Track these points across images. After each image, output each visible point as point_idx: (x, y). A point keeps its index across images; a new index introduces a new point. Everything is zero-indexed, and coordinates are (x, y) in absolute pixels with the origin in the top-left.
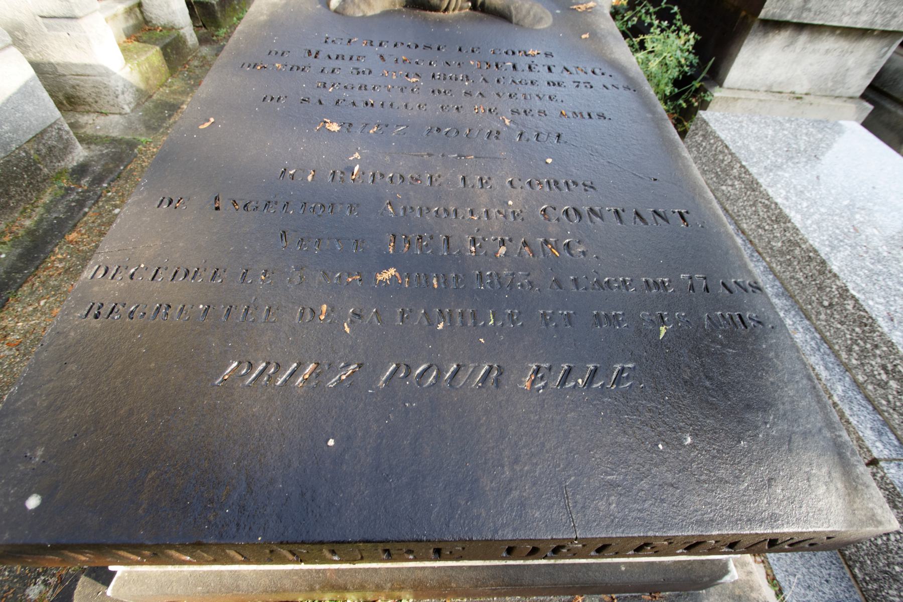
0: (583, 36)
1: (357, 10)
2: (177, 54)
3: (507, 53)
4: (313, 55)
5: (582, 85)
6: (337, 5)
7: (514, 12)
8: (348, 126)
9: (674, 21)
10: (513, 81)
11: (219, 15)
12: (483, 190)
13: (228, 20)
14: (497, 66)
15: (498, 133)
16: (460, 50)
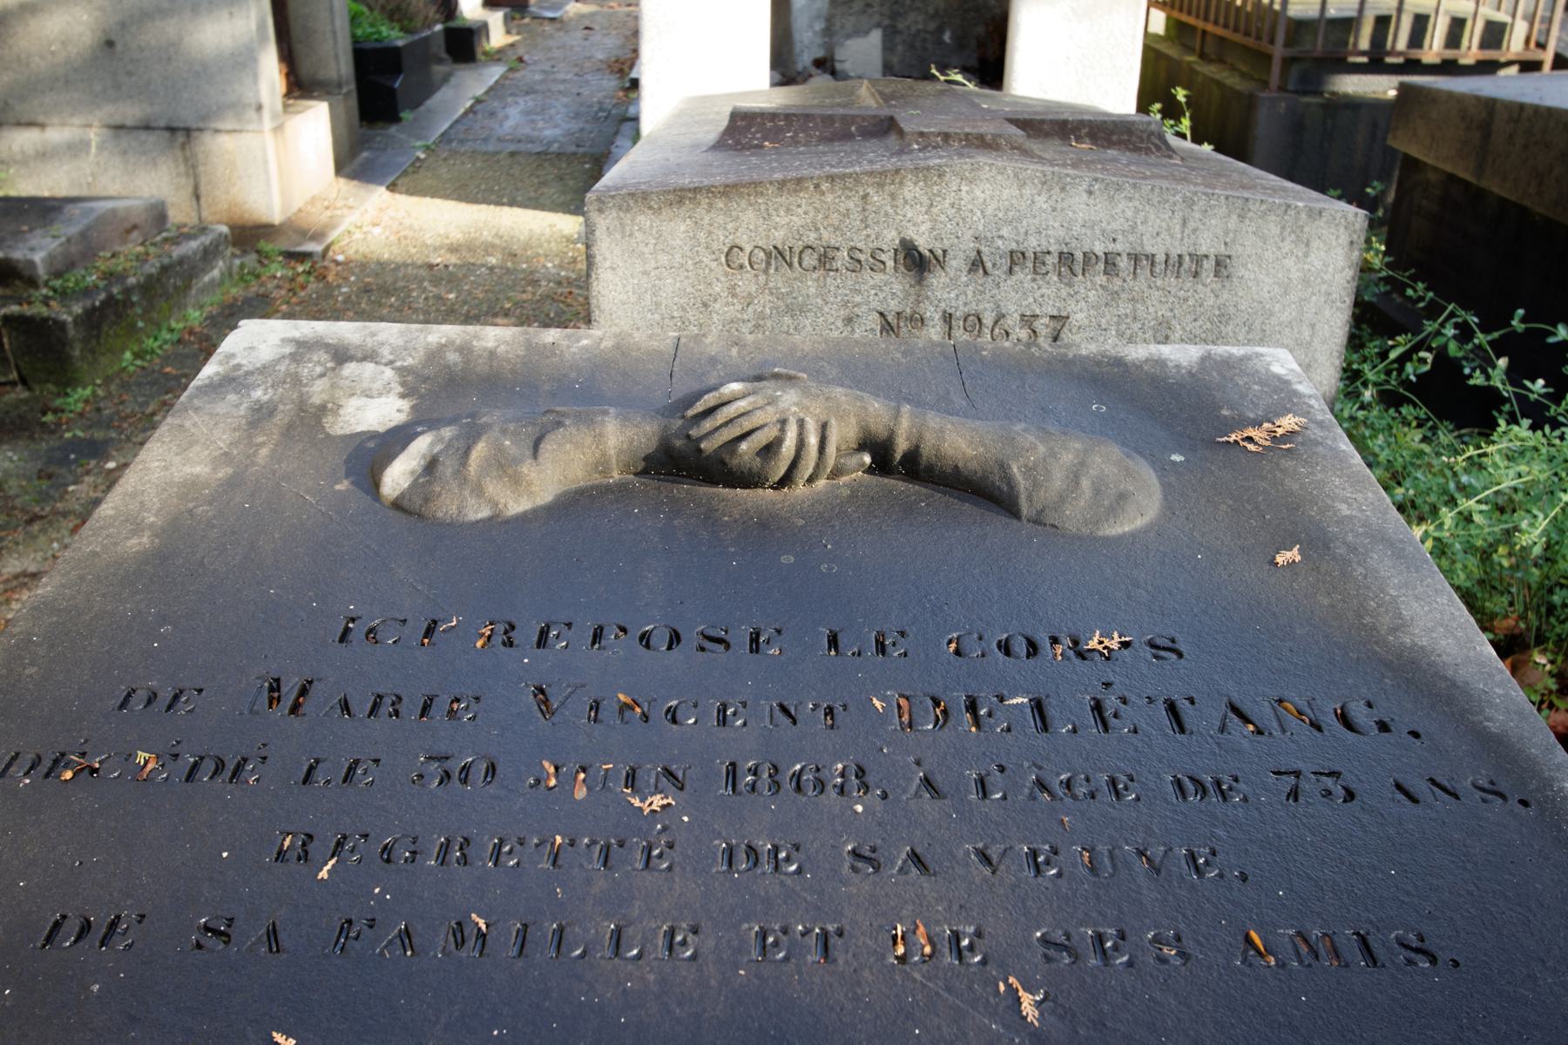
1: (471, 501)
3: (1005, 647)
4: (288, 703)
7: (1022, 483)
10: (1042, 785)
13: (104, 360)
14: (972, 707)
16: (833, 641)
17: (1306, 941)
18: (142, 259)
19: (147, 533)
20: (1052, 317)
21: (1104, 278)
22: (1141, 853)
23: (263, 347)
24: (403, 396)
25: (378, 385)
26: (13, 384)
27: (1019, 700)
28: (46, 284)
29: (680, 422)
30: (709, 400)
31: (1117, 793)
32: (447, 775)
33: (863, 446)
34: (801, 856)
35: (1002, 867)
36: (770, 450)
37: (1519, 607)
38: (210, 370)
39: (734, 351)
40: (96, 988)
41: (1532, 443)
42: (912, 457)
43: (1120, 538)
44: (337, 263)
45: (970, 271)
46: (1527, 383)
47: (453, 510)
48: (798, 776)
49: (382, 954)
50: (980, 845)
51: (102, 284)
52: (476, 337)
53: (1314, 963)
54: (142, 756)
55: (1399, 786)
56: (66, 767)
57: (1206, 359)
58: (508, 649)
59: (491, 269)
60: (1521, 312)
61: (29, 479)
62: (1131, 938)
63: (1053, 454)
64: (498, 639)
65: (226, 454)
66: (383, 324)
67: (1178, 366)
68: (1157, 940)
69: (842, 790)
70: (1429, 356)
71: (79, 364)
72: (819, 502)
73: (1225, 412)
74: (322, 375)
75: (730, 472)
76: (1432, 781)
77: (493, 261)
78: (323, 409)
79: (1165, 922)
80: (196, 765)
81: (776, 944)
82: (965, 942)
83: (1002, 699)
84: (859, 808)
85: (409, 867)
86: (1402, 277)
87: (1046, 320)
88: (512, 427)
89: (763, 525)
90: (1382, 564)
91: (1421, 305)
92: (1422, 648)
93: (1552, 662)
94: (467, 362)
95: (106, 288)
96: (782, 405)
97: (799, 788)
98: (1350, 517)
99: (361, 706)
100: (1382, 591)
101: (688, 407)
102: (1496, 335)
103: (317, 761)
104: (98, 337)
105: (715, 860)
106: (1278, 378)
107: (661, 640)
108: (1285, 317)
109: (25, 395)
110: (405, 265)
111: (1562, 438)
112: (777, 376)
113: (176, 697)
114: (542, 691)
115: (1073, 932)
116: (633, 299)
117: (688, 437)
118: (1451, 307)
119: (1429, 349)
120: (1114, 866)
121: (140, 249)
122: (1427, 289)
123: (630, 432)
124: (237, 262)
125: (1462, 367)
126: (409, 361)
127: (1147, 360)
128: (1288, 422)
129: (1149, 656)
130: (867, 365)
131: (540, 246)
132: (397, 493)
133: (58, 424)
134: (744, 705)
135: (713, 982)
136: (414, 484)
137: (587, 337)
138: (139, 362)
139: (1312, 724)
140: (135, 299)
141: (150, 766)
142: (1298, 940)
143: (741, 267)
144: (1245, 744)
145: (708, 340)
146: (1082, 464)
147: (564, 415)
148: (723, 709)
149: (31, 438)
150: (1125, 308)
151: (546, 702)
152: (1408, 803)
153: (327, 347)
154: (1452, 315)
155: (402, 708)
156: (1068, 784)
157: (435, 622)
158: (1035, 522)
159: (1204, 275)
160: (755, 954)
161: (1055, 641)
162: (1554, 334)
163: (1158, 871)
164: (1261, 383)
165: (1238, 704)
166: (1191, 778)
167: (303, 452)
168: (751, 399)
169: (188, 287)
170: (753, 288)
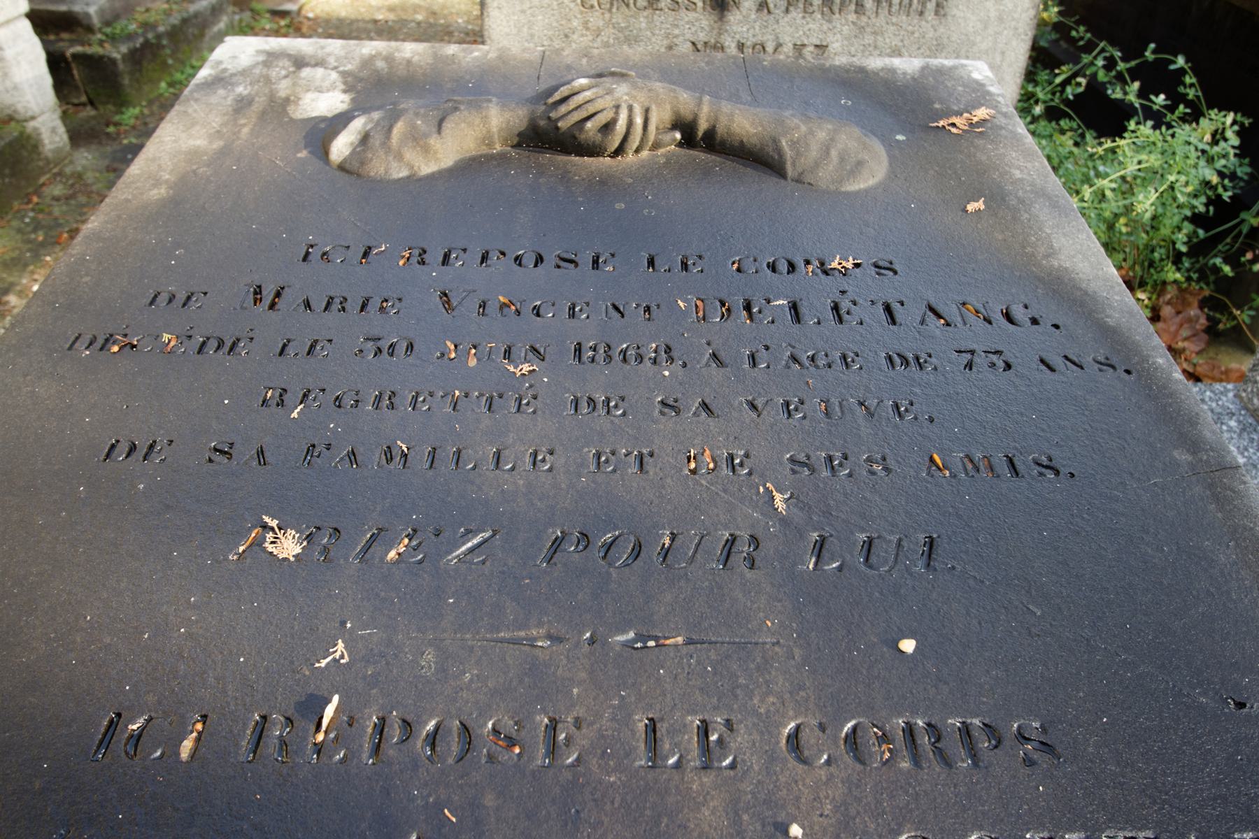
0: (971, 207)
1: (394, 164)
2: (13, 175)
3: (773, 267)
4: (267, 302)
5: (980, 360)
6: (347, 152)
7: (788, 153)
8: (324, 536)
9: (1181, 89)
10: (794, 358)
11: (126, 81)
12: (708, 779)
13: (146, 88)
14: (748, 307)
15: (754, 540)
16: (651, 262)
17: (971, 461)
18: (168, 13)
19: (164, 186)
20: (817, 46)
21: (855, 16)
22: (861, 404)
23: (242, 56)
24: (345, 92)
25: (327, 84)
26: (84, 105)
27: (781, 302)
28: (100, 30)
29: (543, 108)
30: (564, 91)
31: (847, 364)
32: (380, 350)
33: (675, 126)
34: (625, 404)
35: (765, 412)
36: (608, 127)
37: (1130, 262)
38: (204, 73)
39: (584, 61)
40: (142, 486)
41: (1152, 139)
42: (710, 134)
43: (857, 193)
44: (309, 19)
45: (758, 10)
46: (1153, 97)
47: (382, 170)
48: (624, 352)
49: (336, 466)
50: (750, 398)
51: (140, 31)
52: (398, 50)
53: (976, 475)
54: (166, 337)
55: (1042, 361)
56: (114, 343)
57: (924, 68)
58: (422, 267)
59: (419, 23)
60: (1152, 46)
61: (101, 172)
62: (852, 458)
63: (811, 132)
64: (414, 260)
65: (218, 132)
66: (330, 41)
67: (905, 74)
68: (869, 460)
69: (655, 361)
70: (1083, 81)
71: (128, 90)
72: (643, 166)
73: (937, 106)
74: (286, 77)
75: (580, 144)
76: (1066, 357)
77: (419, 17)
78: (287, 100)
79: (876, 448)
80: (204, 343)
81: (607, 461)
82: (737, 461)
83: (769, 302)
84: (667, 373)
85: (354, 410)
86: (1069, 22)
87: (811, 48)
88: (422, 111)
89: (603, 182)
90: (1041, 211)
91: (1081, 43)
92: (1066, 269)
93: (1149, 299)
94: (391, 67)
95: (144, 34)
96: (617, 95)
97: (625, 360)
98: (1021, 180)
99: (318, 305)
100: (1040, 230)
101: (550, 98)
102: (1133, 63)
103: (289, 341)
104: (140, 71)
105: (565, 407)
106: (977, 82)
107: (529, 260)
108: (984, 46)
109: (93, 113)
110: (357, 21)
111: (1173, 136)
112: (613, 74)
113: (189, 298)
114: (446, 295)
115: (811, 454)
116: (514, 31)
117: (549, 118)
118: (1102, 44)
119: (1084, 76)
120: (842, 412)
121: (166, 6)
122: (1087, 31)
123: (507, 115)
124: (237, 17)
125: (1106, 89)
126: (349, 67)
127: (882, 69)
128: (982, 113)
129: (873, 273)
130: (680, 71)
131: (453, 7)
132: (341, 159)
133: (118, 134)
134: (588, 304)
135: (563, 486)
136: (353, 153)
137: (478, 50)
138: (172, 90)
139: (985, 319)
140: (165, 42)
141: (172, 344)
142: (966, 461)
143: (592, 7)
144: (938, 332)
145: (565, 53)
146: (832, 140)
147: (460, 102)
148: (572, 308)
149: (100, 143)
150: (869, 39)
151: (448, 302)
152: (1048, 372)
153: (289, 56)
154: (1103, 50)
155: (347, 306)
156: (813, 359)
157: (370, 248)
158: (797, 181)
159: (927, 14)
160: (593, 468)
161: (808, 262)
162: (1174, 62)
163: (872, 415)
164: (964, 85)
165: (934, 306)
166: (898, 355)
167: (273, 130)
168: (594, 90)
169: (202, 35)
170: (601, 23)
